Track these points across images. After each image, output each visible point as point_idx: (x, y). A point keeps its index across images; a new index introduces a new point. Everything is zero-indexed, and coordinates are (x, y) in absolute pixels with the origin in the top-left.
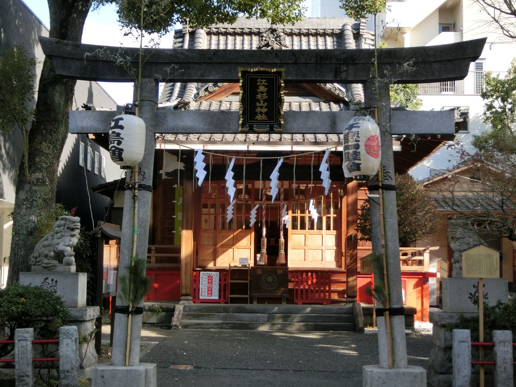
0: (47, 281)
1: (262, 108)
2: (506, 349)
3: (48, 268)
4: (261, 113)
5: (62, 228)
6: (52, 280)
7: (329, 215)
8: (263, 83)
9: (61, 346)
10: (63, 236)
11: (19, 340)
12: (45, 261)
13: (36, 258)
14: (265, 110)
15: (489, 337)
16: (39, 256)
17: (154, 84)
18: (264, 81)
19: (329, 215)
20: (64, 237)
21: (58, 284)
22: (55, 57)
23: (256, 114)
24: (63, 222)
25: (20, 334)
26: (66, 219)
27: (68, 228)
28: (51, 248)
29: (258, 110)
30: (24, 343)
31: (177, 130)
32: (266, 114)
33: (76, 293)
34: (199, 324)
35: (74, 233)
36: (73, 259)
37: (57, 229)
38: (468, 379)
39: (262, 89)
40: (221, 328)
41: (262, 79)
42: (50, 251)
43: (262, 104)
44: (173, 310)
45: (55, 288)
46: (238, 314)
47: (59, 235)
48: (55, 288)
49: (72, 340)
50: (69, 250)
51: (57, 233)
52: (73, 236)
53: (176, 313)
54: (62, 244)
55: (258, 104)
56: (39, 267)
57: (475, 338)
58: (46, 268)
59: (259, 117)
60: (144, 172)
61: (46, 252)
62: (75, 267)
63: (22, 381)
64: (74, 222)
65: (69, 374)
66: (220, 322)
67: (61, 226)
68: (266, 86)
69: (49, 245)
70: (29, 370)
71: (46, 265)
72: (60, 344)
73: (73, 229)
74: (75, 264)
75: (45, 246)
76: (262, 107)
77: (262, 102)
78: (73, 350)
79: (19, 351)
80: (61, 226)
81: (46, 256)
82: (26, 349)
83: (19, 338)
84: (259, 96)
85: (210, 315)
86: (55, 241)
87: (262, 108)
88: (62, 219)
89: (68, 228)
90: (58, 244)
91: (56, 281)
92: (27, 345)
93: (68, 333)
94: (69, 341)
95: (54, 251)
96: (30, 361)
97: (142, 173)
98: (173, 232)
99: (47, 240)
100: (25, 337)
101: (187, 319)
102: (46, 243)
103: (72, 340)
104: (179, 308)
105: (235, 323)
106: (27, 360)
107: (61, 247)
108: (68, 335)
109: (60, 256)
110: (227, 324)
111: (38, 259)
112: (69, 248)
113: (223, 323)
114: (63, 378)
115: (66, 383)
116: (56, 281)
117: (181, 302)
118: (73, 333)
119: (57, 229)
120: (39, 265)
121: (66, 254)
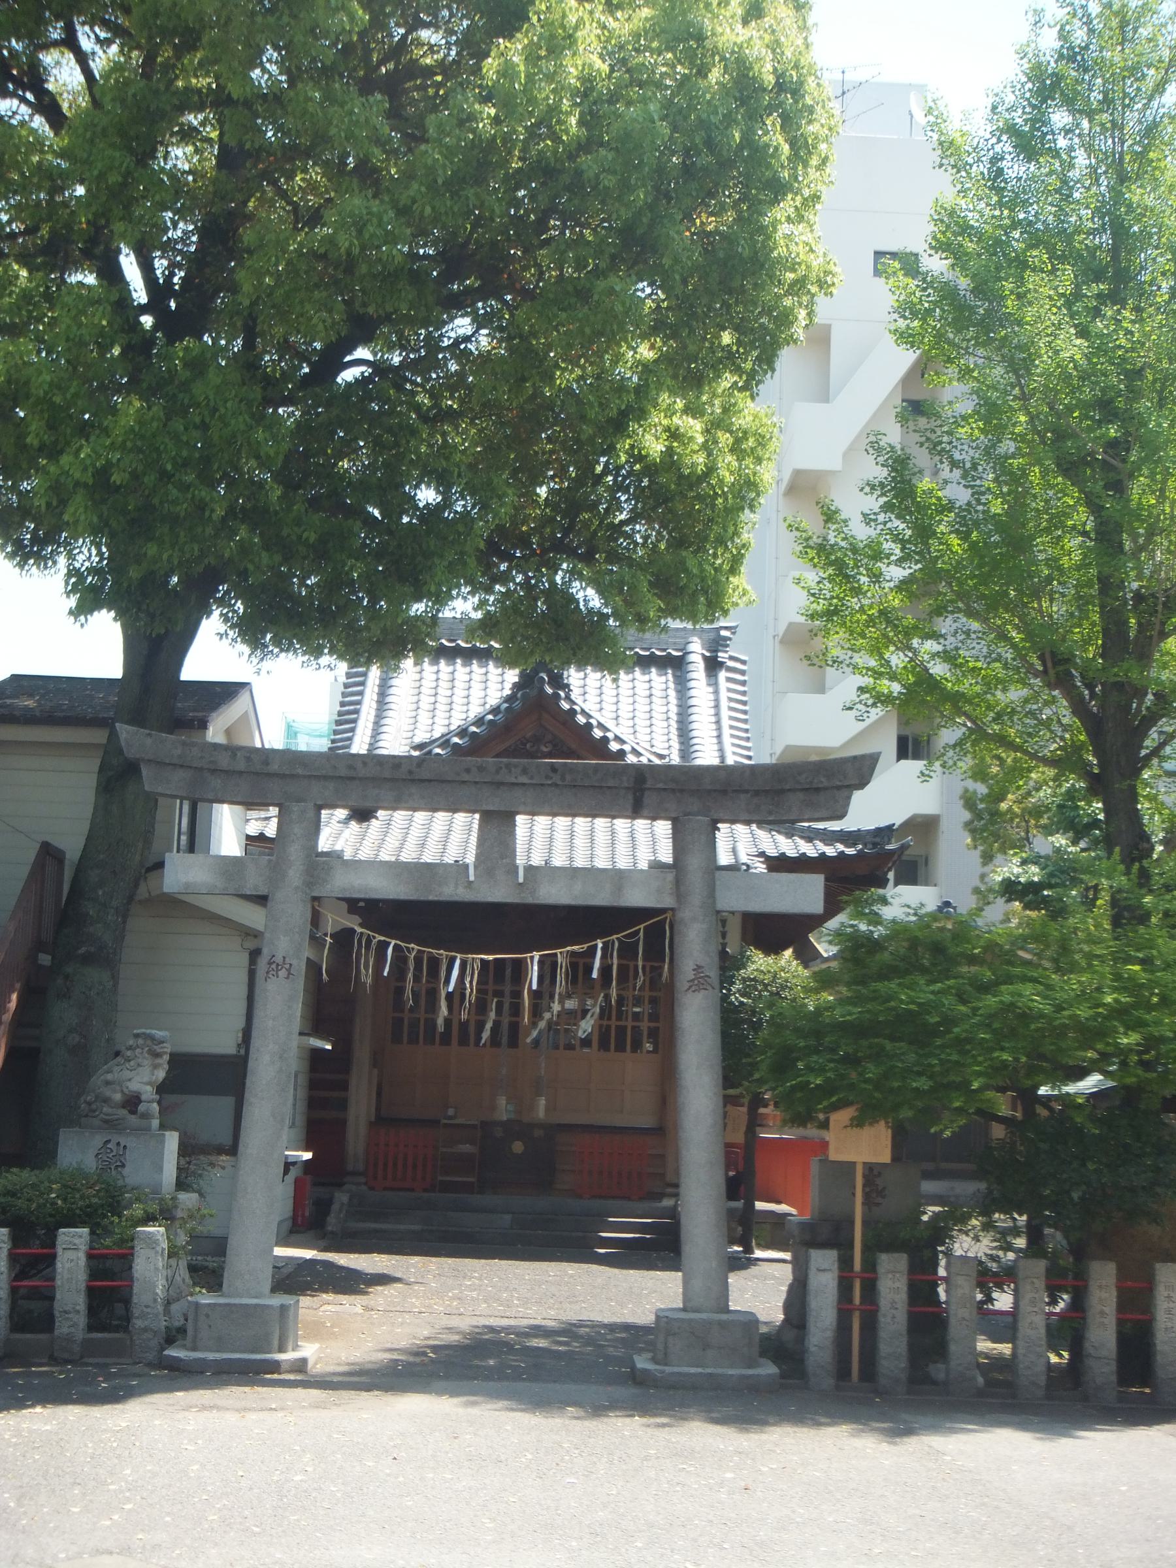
2: (897, 1284)
3: (111, 1124)
7: (652, 1025)
13: (89, 1104)
15: (870, 1266)
17: (311, 814)
19: (652, 1025)
30: (70, 1255)
33: (160, 1169)
34: (376, 1231)
35: (159, 1061)
38: (829, 1334)
44: (330, 1202)
50: (148, 1092)
52: (156, 1067)
53: (335, 1207)
57: (845, 1263)
58: (106, 1122)
70: (363, 1130)
73: (158, 1055)
96: (83, 1286)
98: (308, 1156)
104: (341, 1198)
107: (134, 1086)
108: (151, 1241)
109: (132, 1102)
112: (149, 1088)
117: (346, 1187)
121: (143, 1097)
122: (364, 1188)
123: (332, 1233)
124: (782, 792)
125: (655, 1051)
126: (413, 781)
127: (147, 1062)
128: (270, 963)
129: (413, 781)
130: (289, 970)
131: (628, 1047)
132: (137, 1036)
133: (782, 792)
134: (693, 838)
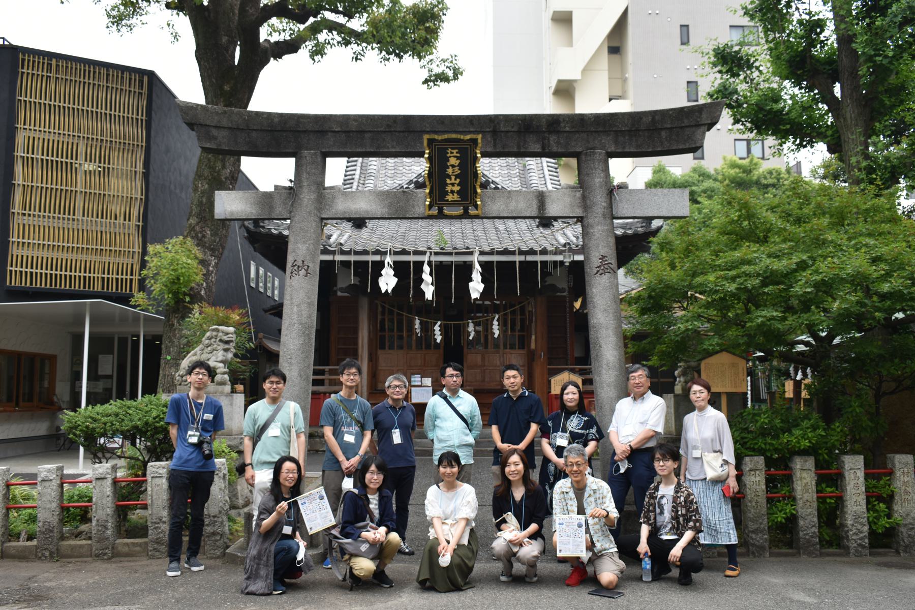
1: (453, 186)
4: (452, 192)
5: (213, 340)
8: (455, 154)
14: (456, 188)
18: (455, 151)
23: (446, 193)
24: (215, 333)
27: (221, 341)
29: (449, 188)
30: (157, 481)
32: (458, 192)
36: (226, 377)
37: (207, 342)
39: (453, 161)
41: (453, 149)
43: (453, 181)
50: (221, 368)
52: (226, 350)
54: (213, 358)
55: (448, 181)
59: (450, 197)
64: (227, 334)
68: (458, 158)
76: (453, 184)
77: (453, 178)
84: (450, 171)
87: (453, 186)
89: (221, 341)
99: (195, 354)
112: (221, 365)
121: (218, 371)
128: (293, 266)
130: (306, 270)
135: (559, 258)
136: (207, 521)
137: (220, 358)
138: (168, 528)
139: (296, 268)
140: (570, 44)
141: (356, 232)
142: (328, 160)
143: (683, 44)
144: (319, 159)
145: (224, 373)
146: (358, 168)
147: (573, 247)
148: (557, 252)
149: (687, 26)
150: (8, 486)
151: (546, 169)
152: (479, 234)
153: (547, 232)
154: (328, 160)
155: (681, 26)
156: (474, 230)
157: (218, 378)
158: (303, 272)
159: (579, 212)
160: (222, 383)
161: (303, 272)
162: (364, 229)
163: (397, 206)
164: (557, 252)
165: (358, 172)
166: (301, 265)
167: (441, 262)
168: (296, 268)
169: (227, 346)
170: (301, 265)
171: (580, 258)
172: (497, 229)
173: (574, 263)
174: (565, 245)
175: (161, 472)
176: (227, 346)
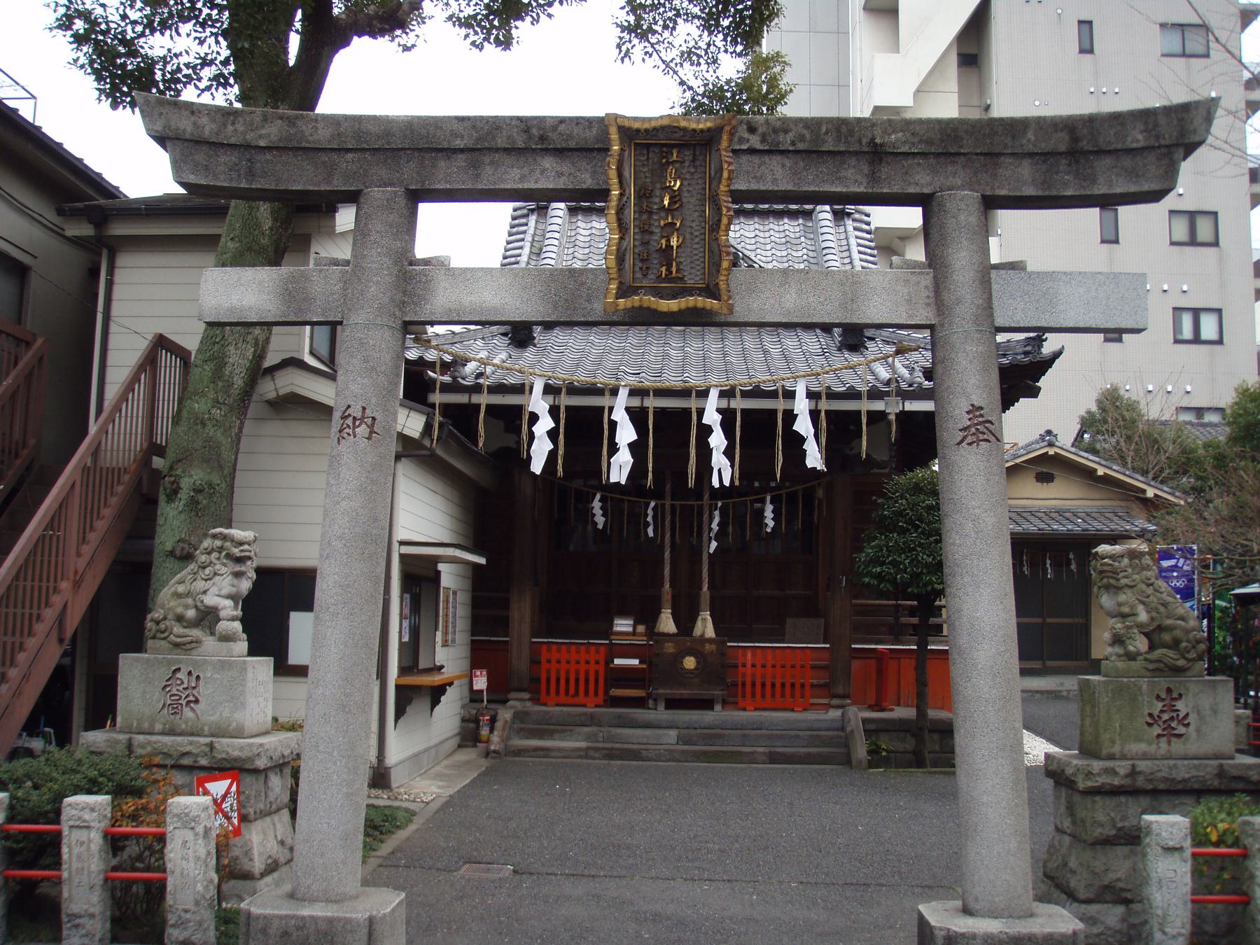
0: (179, 675)
5: (215, 555)
6: (190, 673)
9: (169, 847)
10: (215, 574)
11: (71, 827)
12: (178, 629)
13: (158, 623)
16: (165, 618)
20: (217, 578)
21: (201, 683)
22: (170, 138)
24: (218, 543)
25: (74, 812)
26: (225, 538)
27: (228, 556)
28: (190, 601)
30: (82, 835)
31: (458, 315)
36: (237, 626)
37: (203, 558)
40: (586, 758)
42: (187, 607)
45: (195, 692)
46: (619, 731)
47: (207, 571)
48: (195, 692)
49: (196, 834)
50: (228, 608)
51: (204, 568)
52: (238, 575)
54: (214, 590)
56: (163, 642)
60: (374, 419)
61: (180, 610)
62: (246, 644)
63: (77, 926)
64: (241, 544)
65: (188, 916)
66: (583, 744)
67: (213, 550)
69: (188, 594)
71: (179, 640)
72: (168, 840)
74: (245, 636)
75: (178, 596)
78: (198, 858)
79: (70, 853)
80: (213, 550)
81: (180, 619)
82: (89, 848)
83: (71, 823)
85: (564, 731)
86: (200, 585)
88: (214, 536)
89: (228, 556)
90: (205, 592)
91: (198, 677)
92: (90, 841)
93: (187, 815)
94: (189, 835)
95: (196, 607)
96: (99, 881)
97: (369, 421)
99: (181, 582)
100: (85, 821)
101: (521, 738)
102: (181, 589)
103: (196, 834)
105: (612, 749)
106: (89, 877)
107: (210, 600)
109: (208, 617)
110: (596, 749)
111: (162, 626)
112: (229, 603)
113: (588, 748)
114: (173, 926)
115: (181, 938)
116: (198, 677)
117: (511, 703)
118: (198, 816)
119: (203, 558)
120: (164, 639)
121: (222, 614)
122: (529, 704)
123: (494, 752)
124: (992, 155)
125: (352, 197)
126: (546, 150)
127: (225, 569)
128: (344, 418)
129: (546, 150)
130: (371, 427)
131: (562, 410)
132: (214, 536)
133: (992, 155)
134: (880, 583)
135: (879, 406)
136: (172, 919)
137: (225, 591)
138: (99, 926)
139: (349, 422)
140: (895, 46)
141: (515, 352)
142: (424, 208)
143: (1082, 51)
144: (402, 202)
145: (233, 619)
146: (527, 246)
147: (904, 386)
148: (874, 394)
149: (1090, 23)
150: (1173, 243)
151: (854, 249)
152: (733, 360)
153: (855, 359)
154: (424, 208)
155: (1080, 22)
156: (725, 355)
157: (223, 626)
158: (362, 430)
159: (924, 315)
160: (227, 638)
161: (362, 430)
162: (531, 349)
163: (568, 306)
164: (874, 394)
165: (526, 251)
166: (359, 415)
167: (663, 409)
168: (349, 422)
169: (237, 568)
170: (359, 415)
171: (927, 406)
172: (765, 352)
173: (905, 418)
174: (888, 383)
175: (87, 817)
176: (237, 568)
